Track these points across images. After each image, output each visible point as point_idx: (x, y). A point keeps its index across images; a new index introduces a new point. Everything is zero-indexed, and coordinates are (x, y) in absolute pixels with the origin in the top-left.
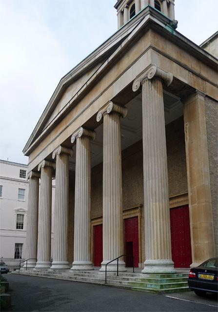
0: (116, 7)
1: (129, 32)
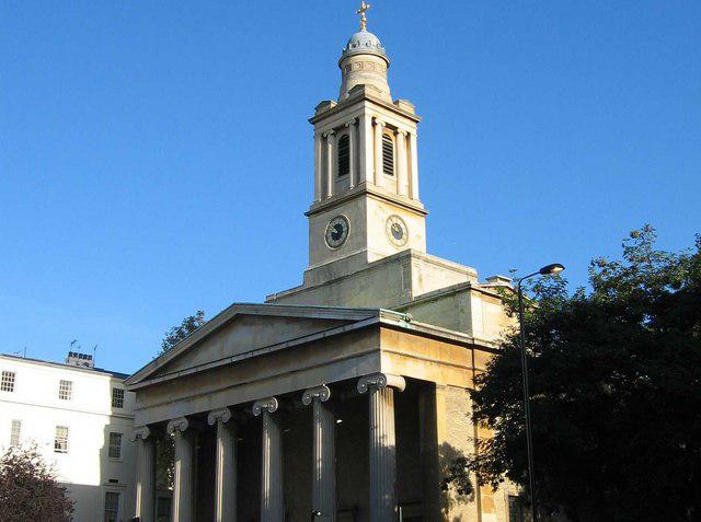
0: (313, 121)
1: (356, 318)
